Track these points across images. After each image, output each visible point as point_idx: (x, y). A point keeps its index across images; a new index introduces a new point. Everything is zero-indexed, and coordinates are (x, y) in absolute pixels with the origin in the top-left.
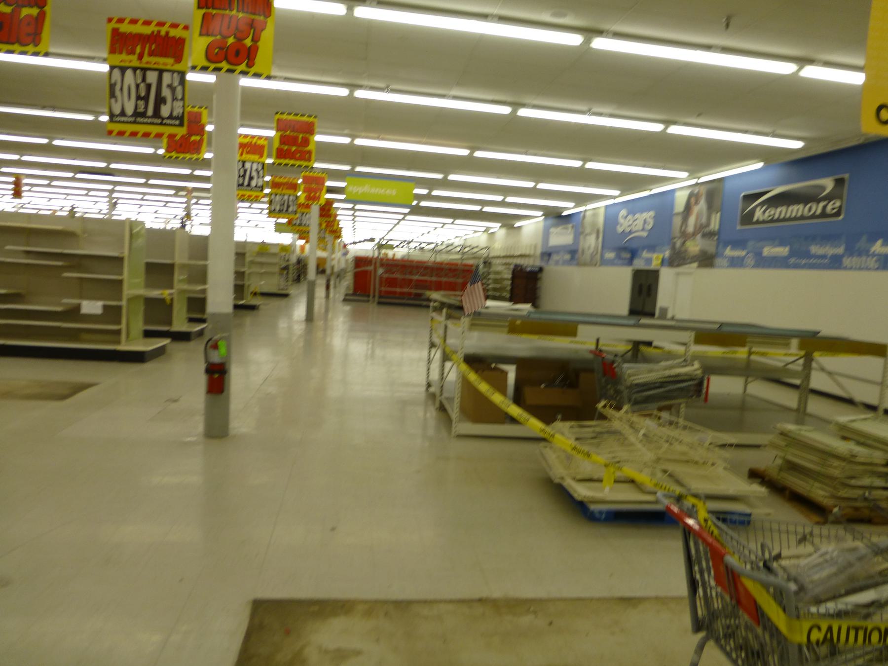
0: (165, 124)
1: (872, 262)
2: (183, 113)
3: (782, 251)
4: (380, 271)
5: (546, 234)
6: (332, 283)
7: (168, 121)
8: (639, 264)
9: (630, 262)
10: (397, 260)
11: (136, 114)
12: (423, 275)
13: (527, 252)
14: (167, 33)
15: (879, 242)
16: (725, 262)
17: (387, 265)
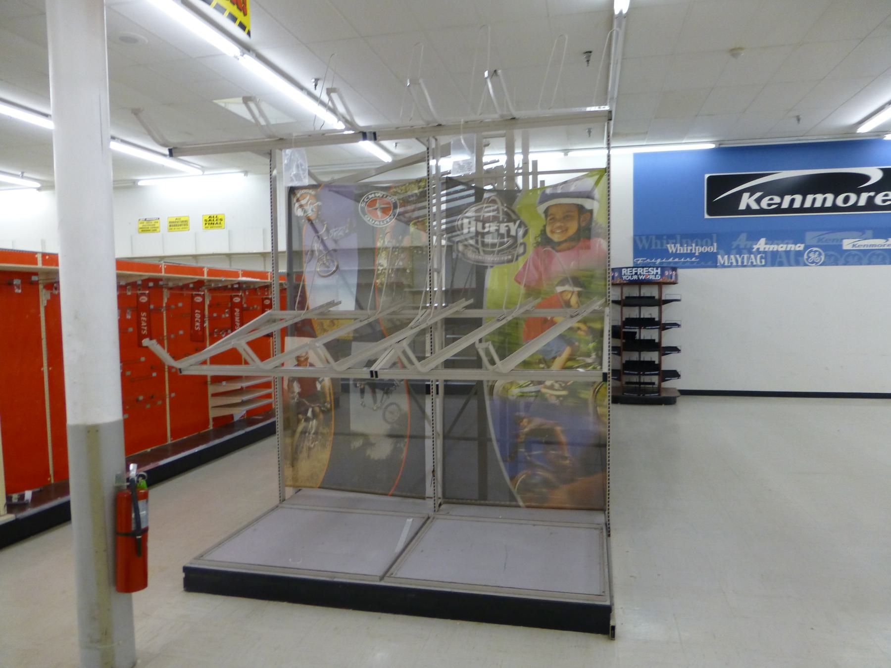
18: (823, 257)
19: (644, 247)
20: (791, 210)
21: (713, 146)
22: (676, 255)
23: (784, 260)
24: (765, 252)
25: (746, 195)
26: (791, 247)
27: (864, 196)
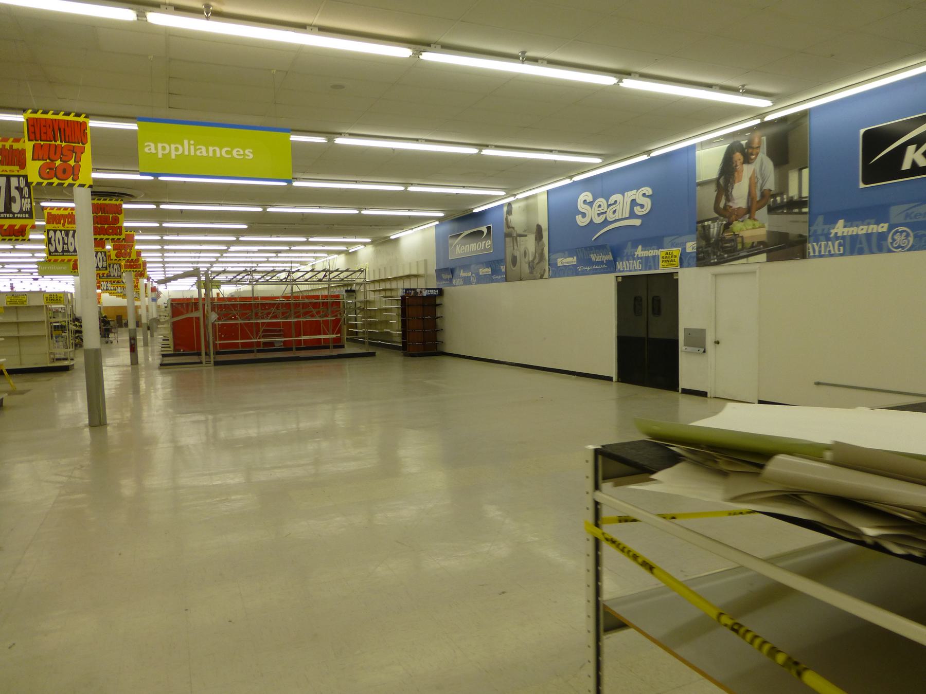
0: (17, 218)
1: (834, 247)
2: (31, 208)
3: (572, 260)
4: (213, 316)
5: (442, 245)
6: (140, 337)
7: (19, 215)
8: (630, 267)
9: (611, 267)
10: (224, 299)
11: (63, 251)
12: (275, 317)
13: (414, 272)
14: (11, 146)
15: (841, 223)
16: (461, 281)
17: (220, 307)
18: (911, 239)
23: (865, 245)
26: (874, 228)
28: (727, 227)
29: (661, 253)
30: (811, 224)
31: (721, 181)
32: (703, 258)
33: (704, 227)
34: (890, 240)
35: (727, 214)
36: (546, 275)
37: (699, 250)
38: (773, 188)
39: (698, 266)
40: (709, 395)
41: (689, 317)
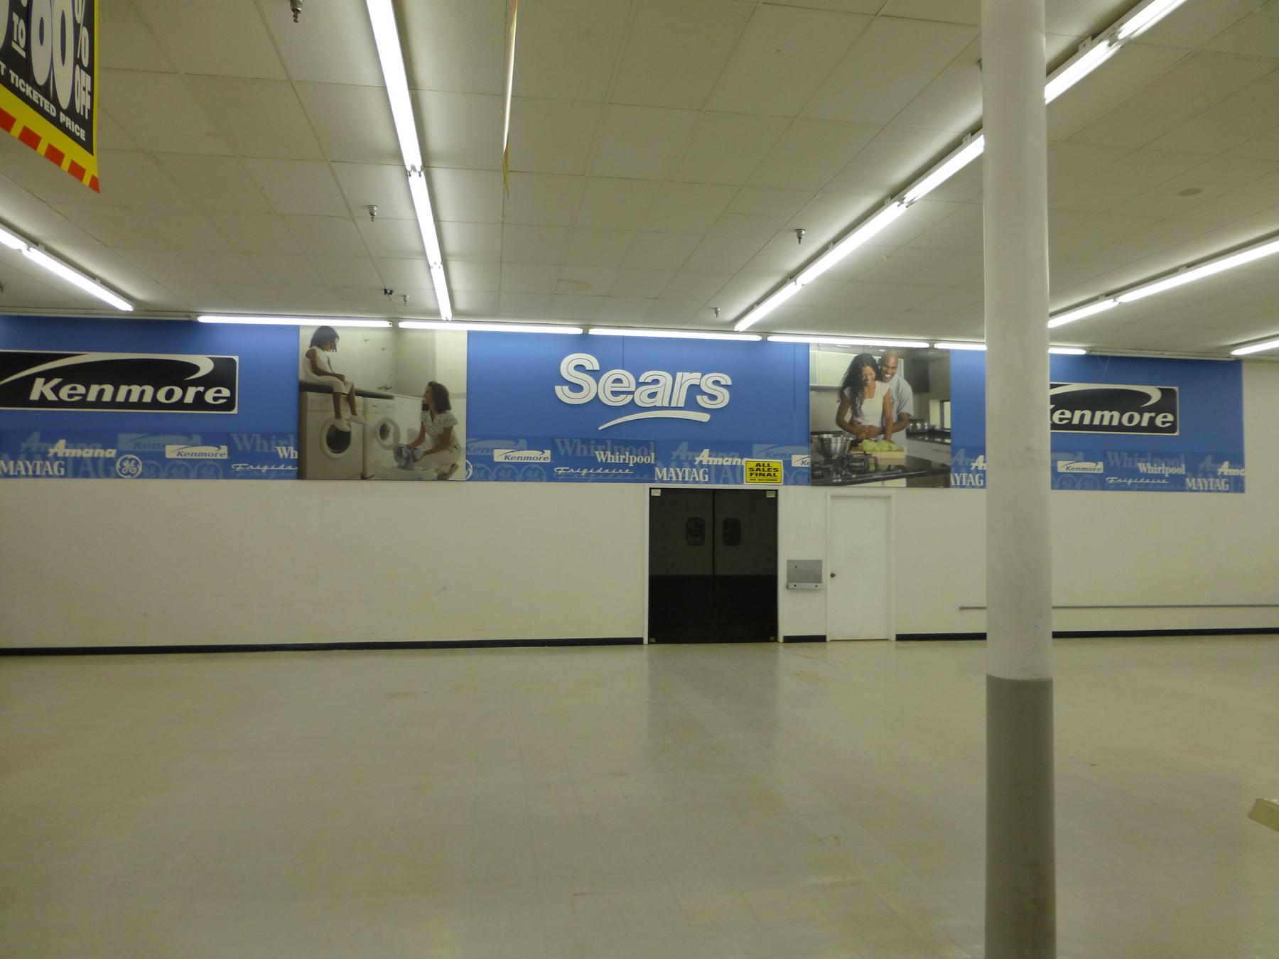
1: (1222, 485)
9: (642, 473)
18: (140, 468)
19: (566, 453)
20: (99, 403)
21: (1083, 352)
22: (1147, 476)
23: (90, 468)
24: (65, 459)
25: (39, 381)
26: (100, 453)
27: (192, 392)
28: (855, 444)
29: (748, 463)
30: (953, 453)
31: (847, 392)
32: (822, 476)
33: (822, 440)
34: (118, 466)
35: (857, 434)
36: (461, 473)
37: (814, 467)
38: (912, 413)
39: (813, 484)
40: (828, 639)
41: (792, 545)
